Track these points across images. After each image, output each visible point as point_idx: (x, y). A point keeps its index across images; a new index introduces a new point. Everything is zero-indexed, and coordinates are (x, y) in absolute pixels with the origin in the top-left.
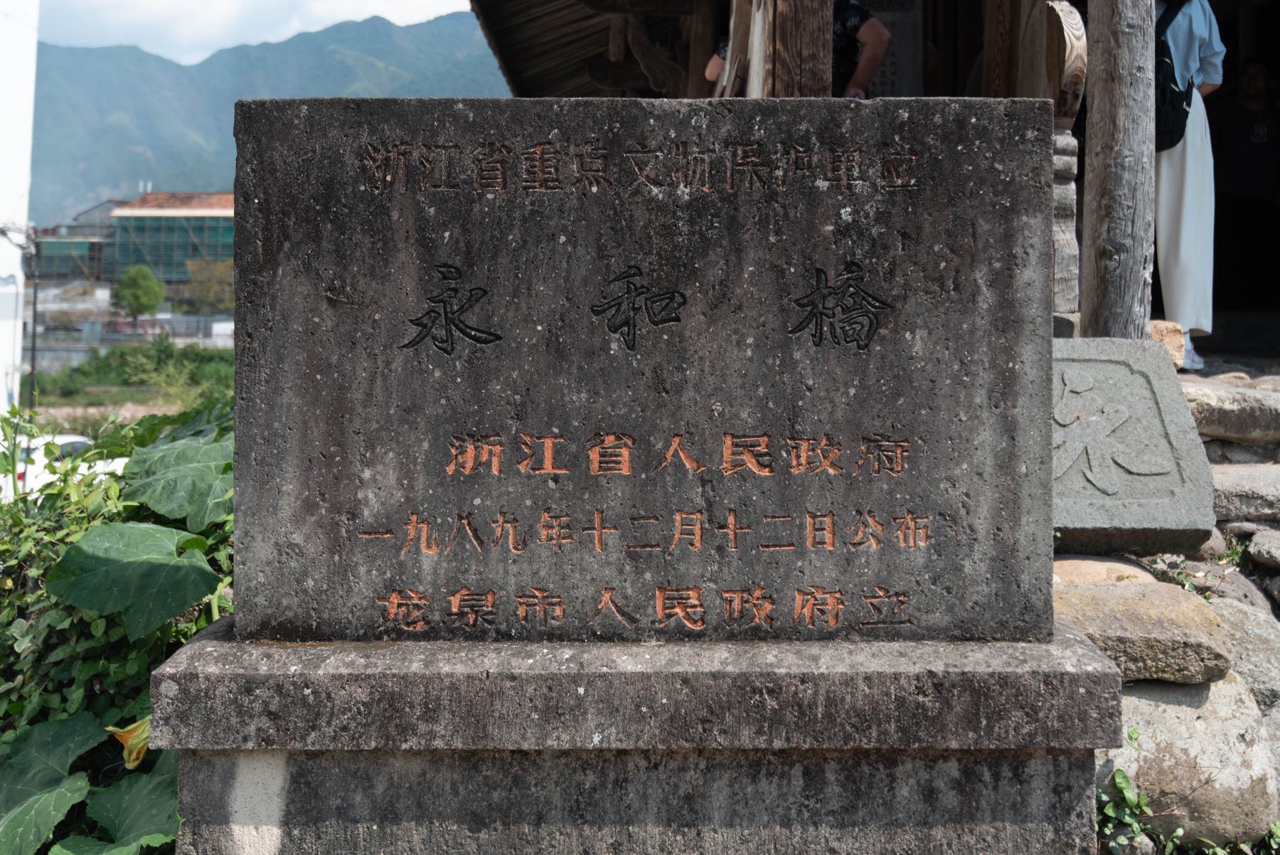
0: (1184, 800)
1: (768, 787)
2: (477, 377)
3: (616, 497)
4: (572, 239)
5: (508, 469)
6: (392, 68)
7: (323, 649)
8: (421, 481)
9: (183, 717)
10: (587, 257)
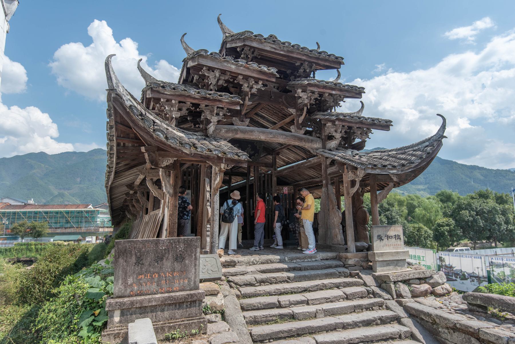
0: (214, 307)
1: (171, 307)
2: (141, 268)
3: (156, 280)
4: (152, 253)
5: (144, 278)
6: (46, 166)
7: (124, 298)
8: (135, 280)
9: (109, 307)
10: (153, 255)
